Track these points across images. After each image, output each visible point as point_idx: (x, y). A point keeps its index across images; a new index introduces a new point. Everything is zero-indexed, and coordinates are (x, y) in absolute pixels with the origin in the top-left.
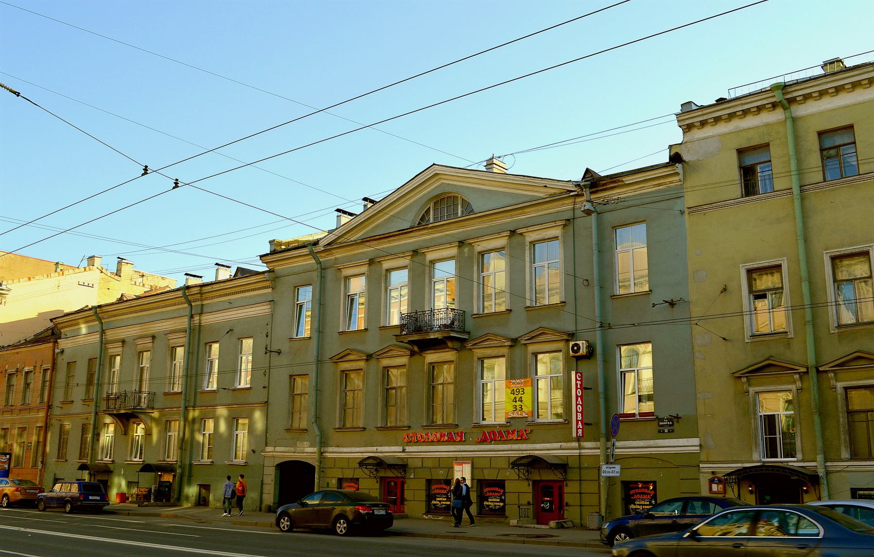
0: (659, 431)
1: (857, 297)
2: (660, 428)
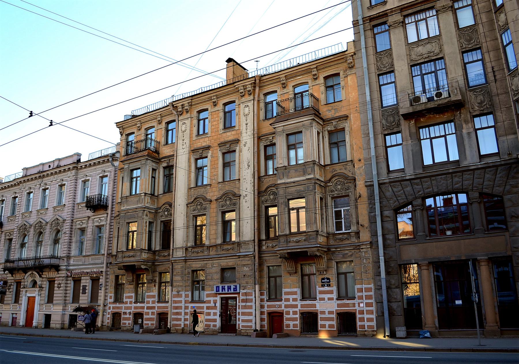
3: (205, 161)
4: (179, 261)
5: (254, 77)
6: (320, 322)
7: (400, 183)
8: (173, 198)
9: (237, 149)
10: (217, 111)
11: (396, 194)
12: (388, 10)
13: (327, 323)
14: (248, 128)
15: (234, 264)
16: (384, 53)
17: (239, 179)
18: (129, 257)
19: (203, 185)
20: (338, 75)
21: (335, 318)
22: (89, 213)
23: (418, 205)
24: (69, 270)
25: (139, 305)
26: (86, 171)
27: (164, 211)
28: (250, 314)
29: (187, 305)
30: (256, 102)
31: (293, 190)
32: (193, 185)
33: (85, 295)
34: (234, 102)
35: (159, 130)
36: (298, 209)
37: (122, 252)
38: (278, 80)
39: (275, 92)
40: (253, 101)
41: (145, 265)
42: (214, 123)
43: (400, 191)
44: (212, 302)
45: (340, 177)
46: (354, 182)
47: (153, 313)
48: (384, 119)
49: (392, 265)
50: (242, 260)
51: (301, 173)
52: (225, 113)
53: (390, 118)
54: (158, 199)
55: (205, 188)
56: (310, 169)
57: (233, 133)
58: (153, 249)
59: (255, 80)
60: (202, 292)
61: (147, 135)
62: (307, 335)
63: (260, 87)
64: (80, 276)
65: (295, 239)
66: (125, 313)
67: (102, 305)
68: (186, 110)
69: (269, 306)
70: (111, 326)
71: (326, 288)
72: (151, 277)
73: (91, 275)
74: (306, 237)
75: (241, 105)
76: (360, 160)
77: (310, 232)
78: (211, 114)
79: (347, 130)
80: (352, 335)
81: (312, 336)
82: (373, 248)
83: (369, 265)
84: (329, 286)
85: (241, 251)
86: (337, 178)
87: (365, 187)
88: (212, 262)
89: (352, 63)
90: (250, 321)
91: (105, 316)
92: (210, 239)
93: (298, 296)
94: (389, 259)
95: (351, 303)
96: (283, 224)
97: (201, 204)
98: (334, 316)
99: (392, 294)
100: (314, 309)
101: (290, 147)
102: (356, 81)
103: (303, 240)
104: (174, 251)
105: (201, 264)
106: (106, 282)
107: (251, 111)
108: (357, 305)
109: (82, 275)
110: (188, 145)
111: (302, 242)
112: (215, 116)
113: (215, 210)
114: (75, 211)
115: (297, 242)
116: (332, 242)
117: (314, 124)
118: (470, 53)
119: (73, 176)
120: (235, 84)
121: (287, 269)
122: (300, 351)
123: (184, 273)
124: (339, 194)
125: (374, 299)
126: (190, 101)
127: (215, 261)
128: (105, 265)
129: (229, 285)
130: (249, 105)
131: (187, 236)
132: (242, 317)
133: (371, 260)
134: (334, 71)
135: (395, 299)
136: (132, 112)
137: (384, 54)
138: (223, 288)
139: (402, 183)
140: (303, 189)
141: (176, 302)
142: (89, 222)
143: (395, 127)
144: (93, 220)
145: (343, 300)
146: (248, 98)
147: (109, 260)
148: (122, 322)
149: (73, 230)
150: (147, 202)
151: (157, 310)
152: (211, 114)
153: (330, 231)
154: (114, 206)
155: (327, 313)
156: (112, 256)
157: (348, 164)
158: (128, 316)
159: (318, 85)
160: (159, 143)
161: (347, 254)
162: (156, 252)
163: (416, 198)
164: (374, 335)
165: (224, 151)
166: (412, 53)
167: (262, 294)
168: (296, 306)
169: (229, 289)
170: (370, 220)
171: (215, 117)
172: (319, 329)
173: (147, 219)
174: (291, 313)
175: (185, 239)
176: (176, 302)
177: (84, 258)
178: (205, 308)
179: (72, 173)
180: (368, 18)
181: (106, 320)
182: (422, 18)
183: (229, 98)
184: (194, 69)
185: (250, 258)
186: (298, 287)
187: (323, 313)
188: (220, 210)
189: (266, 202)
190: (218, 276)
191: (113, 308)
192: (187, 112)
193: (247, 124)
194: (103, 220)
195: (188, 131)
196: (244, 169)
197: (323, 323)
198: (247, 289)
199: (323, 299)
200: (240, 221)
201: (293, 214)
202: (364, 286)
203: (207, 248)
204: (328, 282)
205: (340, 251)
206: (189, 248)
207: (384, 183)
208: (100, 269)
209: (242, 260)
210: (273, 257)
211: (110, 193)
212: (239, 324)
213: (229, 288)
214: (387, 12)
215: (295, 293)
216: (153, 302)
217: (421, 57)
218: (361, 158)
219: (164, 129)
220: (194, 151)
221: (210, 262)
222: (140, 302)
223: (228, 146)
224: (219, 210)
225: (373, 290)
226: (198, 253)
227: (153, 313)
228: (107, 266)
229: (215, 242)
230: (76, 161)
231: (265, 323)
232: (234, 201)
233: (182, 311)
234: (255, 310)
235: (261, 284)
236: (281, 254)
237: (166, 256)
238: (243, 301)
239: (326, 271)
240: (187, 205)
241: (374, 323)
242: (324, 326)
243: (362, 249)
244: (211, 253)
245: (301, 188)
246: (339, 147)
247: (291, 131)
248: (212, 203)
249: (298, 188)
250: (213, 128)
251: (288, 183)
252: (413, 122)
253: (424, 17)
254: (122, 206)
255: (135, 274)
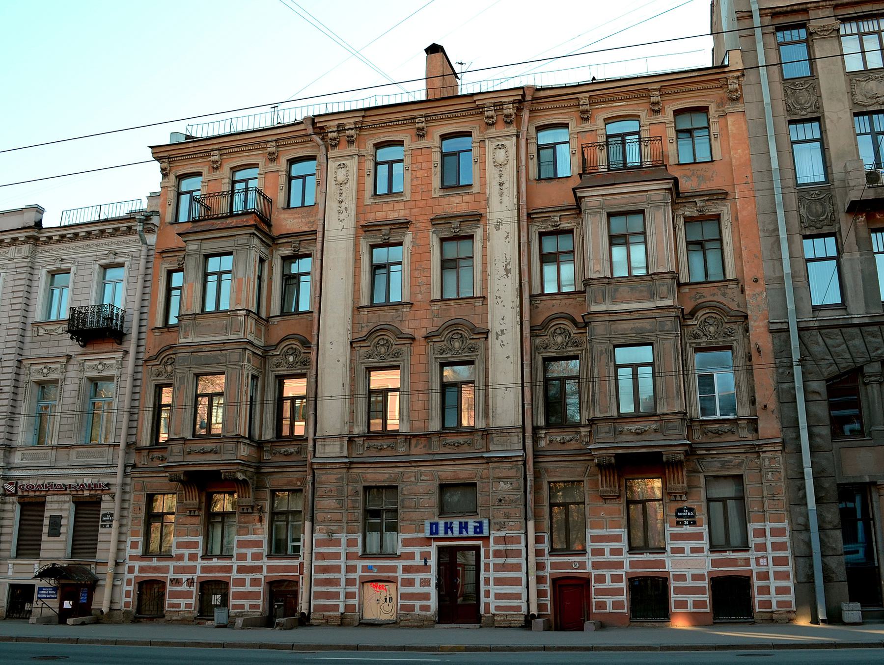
0: (678, 523)
1: (405, 388)
2: (679, 520)
3: (395, 253)
4: (333, 466)
5: (522, 88)
6: (673, 597)
7: (840, 330)
8: (316, 327)
9: (478, 234)
10: (426, 150)
11: (832, 349)
12: (811, 3)
13: (690, 599)
14: (505, 191)
15: (473, 476)
16: (802, 82)
17: (484, 298)
18: (203, 453)
19: (388, 304)
20: (704, 110)
21: (707, 589)
22: (71, 346)
23: (876, 374)
24: (8, 479)
25: (215, 562)
26: (61, 249)
27: (286, 354)
28: (516, 582)
29: (351, 563)
30: (523, 142)
31: (625, 327)
32: (365, 302)
33: (56, 539)
34: (468, 134)
35: (270, 175)
36: (635, 367)
37: (185, 440)
38: (572, 103)
39: (199, 174)
40: (515, 138)
41: (244, 472)
42: (419, 174)
43: (839, 346)
44: (418, 556)
45: (713, 309)
46: (743, 322)
47: (255, 582)
48: (804, 206)
49: (827, 485)
50: (493, 468)
51: (645, 294)
52: (444, 155)
53: (816, 205)
54: (267, 326)
55: (397, 310)
56: (665, 288)
57: (467, 198)
58: (257, 438)
59: (524, 96)
60: (388, 536)
61: (234, 182)
62: (645, 624)
63: (531, 111)
64: (43, 493)
65: (633, 427)
66: (177, 582)
67: (111, 563)
68: (348, 137)
69: (554, 566)
70: (134, 611)
71: (687, 529)
72: (252, 499)
73: (77, 491)
74: (658, 424)
75: (487, 141)
76: (756, 281)
77: (667, 414)
78: (410, 152)
79: (726, 219)
80: (744, 620)
81: (657, 624)
82: (787, 451)
83: (779, 484)
84: (693, 523)
85: (491, 449)
86: (707, 311)
87: (769, 334)
88: (416, 469)
89: (736, 90)
90: (518, 596)
91: (117, 590)
92: (411, 422)
93: (624, 545)
94: (819, 473)
95: (741, 559)
96: (606, 396)
97: (388, 345)
98: (705, 584)
99: (826, 540)
100: (661, 570)
101: (614, 240)
102: (744, 127)
103: (653, 431)
104: (318, 444)
105: (389, 473)
106: (122, 509)
107: (510, 158)
108: (753, 562)
109: (102, 490)
110: (353, 213)
111: (650, 434)
112: (420, 159)
113: (423, 359)
114: (28, 340)
115: (638, 434)
116: (698, 437)
117: (256, 241)
118: (800, 126)
119: (24, 258)
120: (475, 98)
121: (601, 489)
122: (759, 655)
123: (345, 493)
124: (711, 343)
125: (789, 550)
126: (361, 119)
127: (423, 469)
128: (119, 470)
129: (463, 520)
130: (507, 146)
131: (352, 413)
132: (494, 589)
133: (783, 474)
134: (696, 101)
135: (834, 549)
136: (190, 128)
137: (801, 84)
138: (448, 527)
139: (844, 330)
140: (648, 327)
141: (323, 556)
142: (70, 368)
143: (826, 225)
144: (82, 364)
145: (725, 551)
146: (503, 130)
147: (128, 459)
148: (168, 601)
149: (21, 384)
150: (249, 331)
151: (266, 574)
152: (410, 152)
153: (693, 415)
154: (143, 336)
155: (689, 577)
156: (139, 450)
157: (729, 286)
158: (184, 588)
159: (661, 125)
160: (271, 202)
161: (730, 461)
162: (265, 445)
163: (871, 360)
164: (790, 620)
165: (446, 234)
166: (857, 91)
167: (538, 540)
168: (620, 565)
169: (464, 528)
170: (779, 397)
171: (421, 161)
172: (673, 610)
173: (248, 369)
174: (608, 579)
175: (347, 419)
176: (323, 556)
177: (54, 451)
178: (400, 570)
179: (19, 251)
180: (770, 11)
181: (121, 598)
182: (871, 30)
183: (455, 125)
184: (357, 55)
185: (514, 463)
186: (622, 526)
187: (681, 577)
188: (436, 358)
189: (545, 348)
190: (435, 500)
191: (142, 569)
192: (351, 142)
193: (501, 184)
194: (111, 365)
195: (353, 184)
196: (498, 277)
197: (681, 597)
198: (509, 530)
199: (681, 550)
200: (531, 382)
201: (625, 374)
202: (769, 526)
203: (406, 439)
204: (691, 516)
205: (717, 456)
206: (358, 437)
207: (808, 329)
208: (101, 480)
209: (493, 468)
210: (563, 464)
211: (137, 305)
212: (487, 605)
213: (463, 527)
214: (809, 5)
215: (617, 538)
216: (257, 557)
217: (875, 101)
218: (759, 276)
219: (284, 173)
220: (367, 228)
221: (412, 469)
222: (221, 557)
223: (455, 223)
224: (434, 360)
225: (787, 533)
226: (381, 449)
227: (255, 582)
228: (125, 472)
229: (426, 427)
230: (33, 224)
231: (548, 600)
232: (473, 341)
233: (342, 576)
234: (527, 573)
235: (537, 518)
236: (600, 457)
237: (292, 453)
238: (497, 554)
239: (686, 494)
240: (351, 343)
241: (791, 597)
242: (682, 604)
243: (765, 452)
244: (414, 451)
245: (646, 324)
246: (708, 252)
247: (620, 208)
248: (416, 343)
249: (639, 324)
250: (415, 182)
251: (616, 313)
252: (863, 219)
253: (876, 29)
254: (182, 335)
255: (204, 494)
